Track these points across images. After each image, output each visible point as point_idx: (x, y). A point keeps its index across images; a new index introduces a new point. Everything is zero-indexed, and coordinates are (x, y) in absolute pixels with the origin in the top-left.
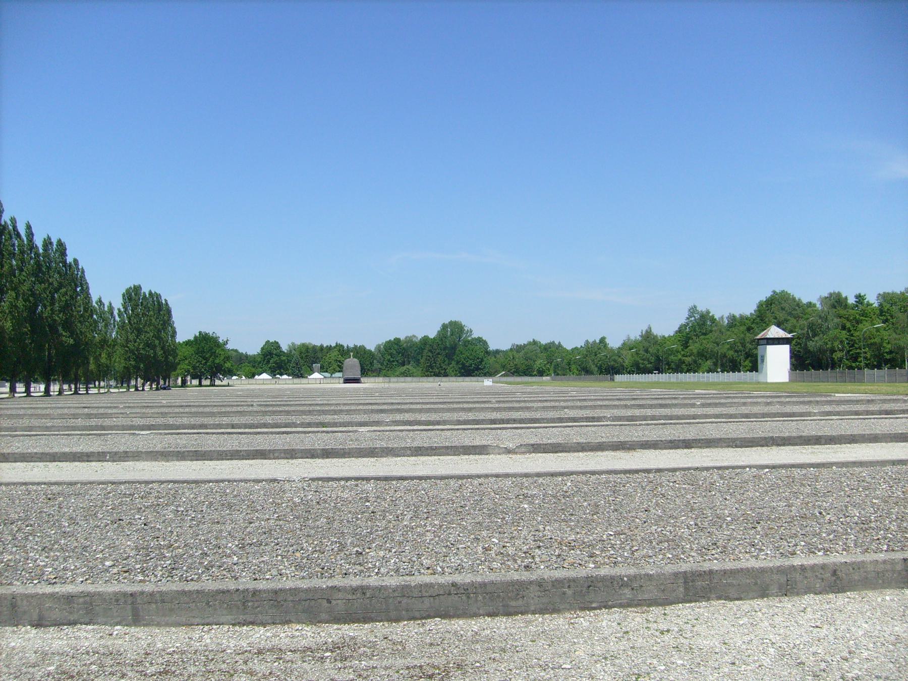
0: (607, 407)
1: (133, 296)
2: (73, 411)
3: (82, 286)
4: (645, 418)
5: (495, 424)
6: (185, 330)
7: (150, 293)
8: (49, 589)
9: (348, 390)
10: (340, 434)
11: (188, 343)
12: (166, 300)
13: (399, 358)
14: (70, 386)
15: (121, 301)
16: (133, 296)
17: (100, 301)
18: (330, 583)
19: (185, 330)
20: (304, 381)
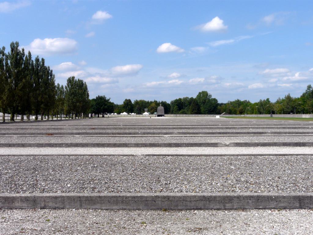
0: (269, 128)
1: (71, 81)
2: (47, 127)
3: (51, 76)
4: (286, 133)
5: (221, 134)
6: (92, 95)
7: (79, 80)
8: (48, 195)
9: (159, 119)
10: (156, 138)
11: (94, 100)
12: (85, 82)
13: (181, 106)
14: (55, 116)
15: (67, 83)
16: (71, 81)
17: (58, 85)
18: (155, 195)
19: (92, 95)
20: (141, 115)
